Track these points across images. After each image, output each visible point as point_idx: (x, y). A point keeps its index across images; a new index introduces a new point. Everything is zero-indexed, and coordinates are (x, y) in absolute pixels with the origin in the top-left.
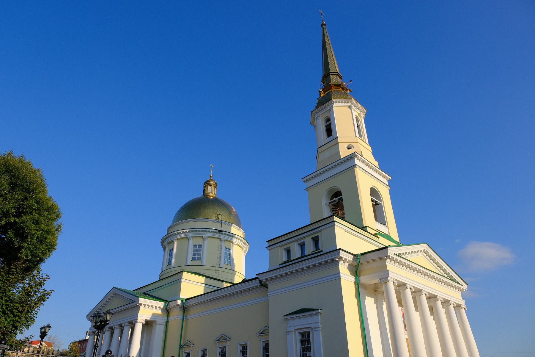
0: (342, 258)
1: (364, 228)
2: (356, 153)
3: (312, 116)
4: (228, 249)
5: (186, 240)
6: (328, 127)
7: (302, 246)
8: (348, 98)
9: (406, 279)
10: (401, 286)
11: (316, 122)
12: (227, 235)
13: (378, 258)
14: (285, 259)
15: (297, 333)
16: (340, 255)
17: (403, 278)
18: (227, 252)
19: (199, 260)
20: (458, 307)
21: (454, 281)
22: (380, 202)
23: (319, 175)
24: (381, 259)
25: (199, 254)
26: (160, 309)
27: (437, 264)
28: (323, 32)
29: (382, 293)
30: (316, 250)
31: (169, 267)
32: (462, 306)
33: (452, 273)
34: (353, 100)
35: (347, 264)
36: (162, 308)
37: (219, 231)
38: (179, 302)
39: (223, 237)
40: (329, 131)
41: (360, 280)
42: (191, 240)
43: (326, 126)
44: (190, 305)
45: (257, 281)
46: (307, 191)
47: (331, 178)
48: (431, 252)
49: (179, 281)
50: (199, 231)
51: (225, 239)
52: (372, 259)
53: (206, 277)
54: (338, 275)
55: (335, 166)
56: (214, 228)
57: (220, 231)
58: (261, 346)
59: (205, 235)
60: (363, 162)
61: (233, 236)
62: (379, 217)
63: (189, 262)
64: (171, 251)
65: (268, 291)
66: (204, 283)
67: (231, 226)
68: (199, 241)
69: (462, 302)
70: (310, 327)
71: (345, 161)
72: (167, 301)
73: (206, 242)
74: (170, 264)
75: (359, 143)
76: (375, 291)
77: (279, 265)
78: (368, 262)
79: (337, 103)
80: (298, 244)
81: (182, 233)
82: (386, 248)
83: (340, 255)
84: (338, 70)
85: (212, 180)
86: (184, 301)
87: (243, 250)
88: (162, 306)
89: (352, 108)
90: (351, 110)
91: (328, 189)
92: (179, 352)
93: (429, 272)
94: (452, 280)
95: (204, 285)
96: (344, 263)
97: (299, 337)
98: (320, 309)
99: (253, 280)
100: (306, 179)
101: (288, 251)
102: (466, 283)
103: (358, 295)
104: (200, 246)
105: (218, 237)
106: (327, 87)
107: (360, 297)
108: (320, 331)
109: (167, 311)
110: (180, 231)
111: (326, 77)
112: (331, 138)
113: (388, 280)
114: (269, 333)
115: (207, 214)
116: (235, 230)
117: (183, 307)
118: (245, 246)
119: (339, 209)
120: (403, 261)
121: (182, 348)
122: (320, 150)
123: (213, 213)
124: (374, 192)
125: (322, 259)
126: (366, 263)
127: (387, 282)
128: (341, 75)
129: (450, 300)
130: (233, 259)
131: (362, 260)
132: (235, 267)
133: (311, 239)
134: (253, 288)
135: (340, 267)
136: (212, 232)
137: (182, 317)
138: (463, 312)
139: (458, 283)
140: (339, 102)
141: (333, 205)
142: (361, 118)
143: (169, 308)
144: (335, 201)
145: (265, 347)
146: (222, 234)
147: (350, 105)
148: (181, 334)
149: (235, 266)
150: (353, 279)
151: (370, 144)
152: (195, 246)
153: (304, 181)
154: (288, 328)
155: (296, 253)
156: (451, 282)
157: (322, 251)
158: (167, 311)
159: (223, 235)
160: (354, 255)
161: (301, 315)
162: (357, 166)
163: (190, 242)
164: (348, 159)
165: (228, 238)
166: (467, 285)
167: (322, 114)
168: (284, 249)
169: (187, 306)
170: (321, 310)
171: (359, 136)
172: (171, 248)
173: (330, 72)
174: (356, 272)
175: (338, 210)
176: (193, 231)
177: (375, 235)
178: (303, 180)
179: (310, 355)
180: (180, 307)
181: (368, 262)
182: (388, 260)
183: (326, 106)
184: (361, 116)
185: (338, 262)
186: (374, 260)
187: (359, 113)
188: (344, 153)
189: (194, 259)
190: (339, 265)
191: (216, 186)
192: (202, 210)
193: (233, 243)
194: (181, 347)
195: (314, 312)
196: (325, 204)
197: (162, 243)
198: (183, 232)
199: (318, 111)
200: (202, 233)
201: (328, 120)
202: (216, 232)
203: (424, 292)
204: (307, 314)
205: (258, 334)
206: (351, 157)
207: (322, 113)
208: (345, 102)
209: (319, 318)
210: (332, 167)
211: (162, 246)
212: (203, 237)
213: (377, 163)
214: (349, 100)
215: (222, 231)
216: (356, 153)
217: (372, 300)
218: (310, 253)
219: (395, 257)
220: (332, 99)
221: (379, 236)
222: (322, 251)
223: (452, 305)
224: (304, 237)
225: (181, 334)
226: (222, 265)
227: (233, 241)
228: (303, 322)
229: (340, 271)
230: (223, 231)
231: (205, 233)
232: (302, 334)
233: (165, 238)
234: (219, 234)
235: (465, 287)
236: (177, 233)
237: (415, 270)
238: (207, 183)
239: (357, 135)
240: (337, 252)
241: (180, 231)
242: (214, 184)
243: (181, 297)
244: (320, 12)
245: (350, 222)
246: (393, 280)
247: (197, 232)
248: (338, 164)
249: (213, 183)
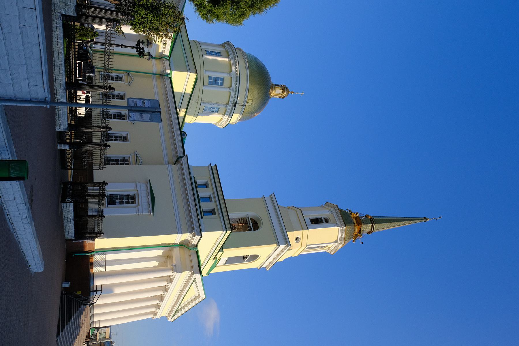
0: (195, 237)
1: (222, 249)
2: (290, 247)
3: (333, 205)
4: (218, 111)
5: (228, 70)
6: (320, 220)
7: (209, 199)
8: (345, 240)
9: (169, 296)
10: (170, 280)
11: (326, 208)
12: (231, 111)
13: (192, 265)
14: (199, 182)
15: (135, 192)
16: (196, 236)
17: (176, 281)
18: (215, 109)
19: (209, 83)
20: (155, 314)
21: (175, 313)
22: (246, 261)
23: (275, 210)
24: (192, 267)
25: (214, 84)
26: (163, 51)
27: (189, 303)
28: (418, 219)
29: (165, 261)
30: (203, 212)
31: (204, 52)
32: (171, 283)
33: (181, 313)
34: (342, 245)
35: (190, 239)
36: (164, 53)
37: (236, 103)
38: (168, 71)
39: (229, 107)
40: (317, 221)
41: (176, 248)
42: (228, 75)
43: (321, 219)
44: (165, 82)
45: (182, 155)
46: (262, 198)
47: (271, 222)
48: (198, 300)
49: (188, 70)
50: (236, 84)
51: (224, 119)
52: (192, 260)
53: (191, 95)
54: (180, 232)
55: (281, 226)
56: (238, 98)
57: (235, 105)
58: (126, 155)
59: (233, 89)
60: (282, 251)
61: (230, 115)
62: (230, 261)
63: (207, 74)
64: (219, 54)
65: (172, 165)
66: (186, 92)
67: (240, 114)
68: (227, 83)
69: (158, 316)
70: (139, 205)
71: (284, 235)
72: (170, 58)
73: (226, 90)
74: (208, 53)
75: (301, 248)
76: (168, 257)
77: (194, 177)
78: (190, 256)
79: (341, 231)
80: (211, 195)
81: (235, 67)
82: (200, 272)
83: (196, 236)
84: (376, 231)
85: (288, 94)
86: (169, 76)
87: (217, 123)
88: (165, 53)
89: (335, 243)
90: (333, 243)
91: (261, 218)
92: (123, 71)
93: (181, 298)
94: (176, 312)
95: (183, 92)
96: (190, 237)
97: (131, 193)
98: (153, 215)
99: (182, 146)
100: (273, 197)
101: (206, 185)
102: (173, 321)
103: (163, 246)
104: (222, 84)
105: (230, 103)
106: (360, 221)
107: (162, 247)
108: (135, 214)
109: (161, 57)
110: (237, 62)
111: (370, 220)
112: (309, 222)
113: (174, 272)
114: (137, 165)
115: (253, 92)
116: (236, 117)
117: (164, 74)
118: (222, 124)
119: (243, 224)
120: (190, 283)
121: (127, 73)
122: (299, 211)
123: (254, 97)
124: (255, 257)
125: (194, 219)
126: (189, 254)
127: (172, 270)
128: (370, 233)
129: (159, 309)
130: (208, 115)
131: (193, 252)
132: (201, 116)
133: (213, 208)
134: (176, 148)
135: (187, 234)
136: (235, 97)
137: (154, 73)
138: (151, 316)
139: (173, 316)
140: (342, 232)
141: (246, 220)
142: (326, 249)
143: (163, 61)
144: (250, 224)
145: (125, 159)
146: (233, 106)
147: (338, 242)
148: (139, 72)
149: (202, 116)
150: (178, 242)
151: (300, 256)
152: (222, 79)
153: (271, 195)
154: (139, 184)
155: (203, 193)
156: (174, 312)
157: (202, 218)
158: (161, 58)
159: (231, 107)
160: (196, 246)
161: (149, 197)
162: (278, 246)
163: (227, 74)
164: (285, 239)
165: (228, 111)
166: (172, 322)
167: (333, 215)
168: (208, 181)
169: (165, 79)
170: (152, 215)
171: (308, 248)
172: (222, 54)
173: (375, 224)
174: (183, 245)
175: (243, 224)
176: (237, 78)
177: (216, 258)
178: (273, 195)
179: (116, 203)
180: (164, 72)
181: (190, 256)
182: (190, 273)
183: (340, 220)
184: (328, 250)
185: (192, 233)
186: (191, 261)
187: (331, 248)
188: (292, 235)
189: (209, 78)
190: (189, 234)
191: (282, 97)
192: (257, 86)
193: (224, 115)
194: (128, 72)
195: (151, 209)
196: (248, 214)
197: (228, 43)
198: (236, 68)
199: (337, 211)
200: (235, 86)
201: (327, 221)
202: (234, 100)
203: (165, 293)
204: (150, 203)
205: (136, 152)
206: (287, 242)
207: (335, 216)
208: (341, 238)
209: (146, 213)
210: (280, 223)
211: (225, 43)
212: (230, 88)
213: (282, 261)
214: (343, 242)
215: (235, 106)
216: (290, 247)
217: (161, 254)
218: (201, 207)
219: (193, 279)
220: (346, 226)
221: (214, 260)
222: (202, 218)
223: (164, 294)
224: (216, 202)
225: (139, 72)
226: (203, 105)
227: (225, 116)
228: (143, 198)
229: (183, 234)
230: (235, 107)
231: (235, 90)
232: (133, 197)
233: (232, 46)
234: (232, 103)
235: (170, 320)
236: (236, 61)
237: (182, 291)
238: (285, 88)
239: (308, 247)
240: (199, 233)
241: (237, 62)
242: (284, 95)
243: (173, 72)
244: (440, 217)
245: (228, 239)
246: (174, 275)
247: (236, 82)
248: (282, 229)
249: (285, 94)
